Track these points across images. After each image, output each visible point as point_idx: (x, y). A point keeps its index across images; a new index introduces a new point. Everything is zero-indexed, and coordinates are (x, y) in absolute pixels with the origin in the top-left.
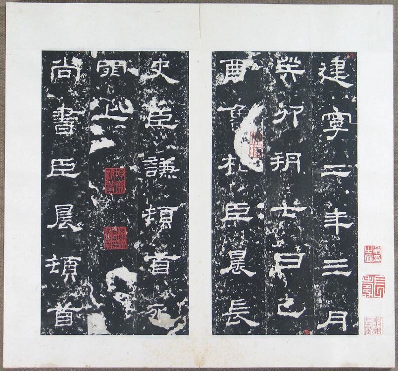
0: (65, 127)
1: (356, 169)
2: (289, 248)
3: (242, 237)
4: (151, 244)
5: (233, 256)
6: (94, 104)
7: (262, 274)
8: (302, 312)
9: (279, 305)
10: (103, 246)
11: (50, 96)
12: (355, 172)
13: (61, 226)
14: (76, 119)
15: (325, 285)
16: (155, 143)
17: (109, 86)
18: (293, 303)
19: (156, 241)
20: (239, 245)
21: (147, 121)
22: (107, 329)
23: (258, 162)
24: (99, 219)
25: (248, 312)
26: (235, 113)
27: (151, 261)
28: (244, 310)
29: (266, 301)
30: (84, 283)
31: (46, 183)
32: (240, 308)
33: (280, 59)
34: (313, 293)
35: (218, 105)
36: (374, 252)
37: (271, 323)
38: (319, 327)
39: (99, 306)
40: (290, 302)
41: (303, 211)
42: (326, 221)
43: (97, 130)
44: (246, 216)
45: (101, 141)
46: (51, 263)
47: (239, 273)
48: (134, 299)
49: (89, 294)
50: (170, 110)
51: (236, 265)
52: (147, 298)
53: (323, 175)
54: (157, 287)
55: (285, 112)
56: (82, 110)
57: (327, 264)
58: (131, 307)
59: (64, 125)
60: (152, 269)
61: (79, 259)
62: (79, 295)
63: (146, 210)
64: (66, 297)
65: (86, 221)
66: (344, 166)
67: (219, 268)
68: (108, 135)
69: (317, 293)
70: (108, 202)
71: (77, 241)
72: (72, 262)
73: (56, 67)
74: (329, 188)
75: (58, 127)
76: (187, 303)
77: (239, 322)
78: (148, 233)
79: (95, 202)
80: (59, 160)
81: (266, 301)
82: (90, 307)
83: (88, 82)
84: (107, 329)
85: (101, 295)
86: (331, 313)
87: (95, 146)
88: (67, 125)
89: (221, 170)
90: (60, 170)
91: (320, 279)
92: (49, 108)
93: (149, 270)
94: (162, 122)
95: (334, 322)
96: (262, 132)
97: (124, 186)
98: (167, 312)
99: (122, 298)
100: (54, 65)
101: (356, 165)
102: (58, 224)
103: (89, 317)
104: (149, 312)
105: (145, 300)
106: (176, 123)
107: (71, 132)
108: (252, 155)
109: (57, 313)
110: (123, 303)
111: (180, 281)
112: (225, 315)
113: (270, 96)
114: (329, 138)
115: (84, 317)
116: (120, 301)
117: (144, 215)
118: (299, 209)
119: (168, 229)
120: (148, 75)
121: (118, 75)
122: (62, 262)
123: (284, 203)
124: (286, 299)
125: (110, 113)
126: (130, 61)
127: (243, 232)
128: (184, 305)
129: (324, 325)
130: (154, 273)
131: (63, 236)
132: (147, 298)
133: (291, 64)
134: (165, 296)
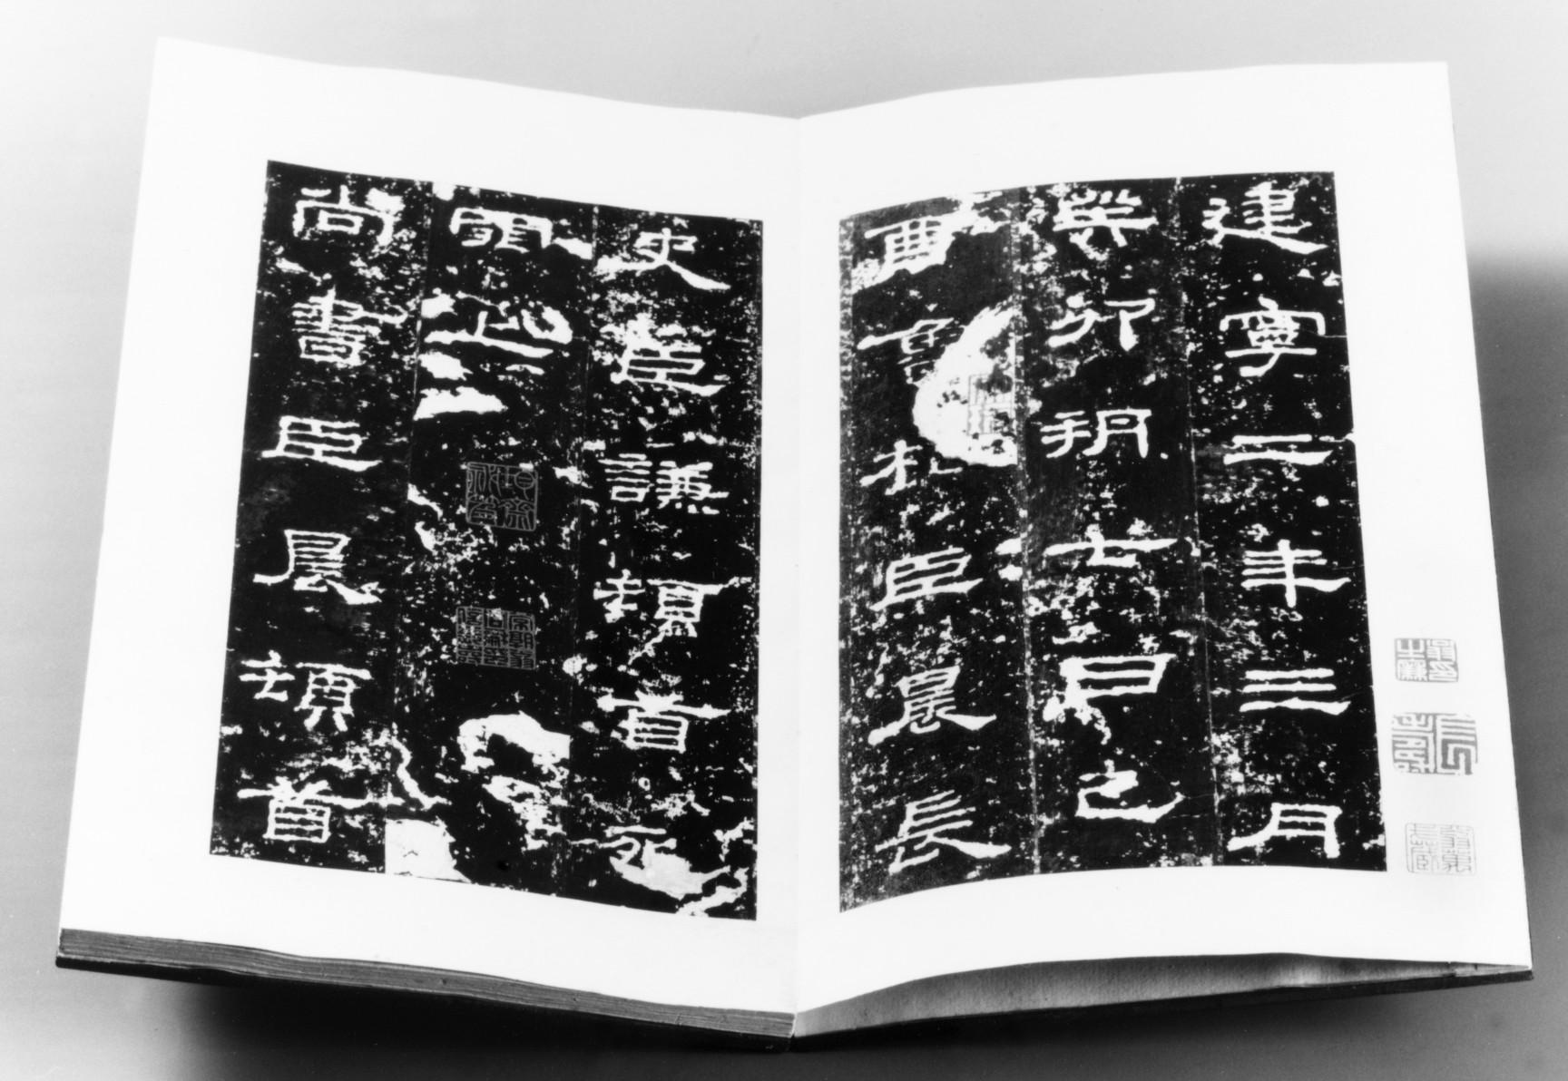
0: (335, 345)
1: (1350, 447)
2: (1116, 638)
3: (945, 635)
4: (622, 668)
5: (912, 690)
6: (438, 304)
7: (1012, 721)
8: (1166, 809)
9: (1082, 793)
10: (450, 651)
11: (286, 265)
12: (1346, 456)
13: (302, 584)
14: (375, 331)
15: (1255, 736)
16: (643, 421)
17: (491, 269)
18: (1136, 784)
19: (640, 663)
20: (933, 655)
21: (616, 367)
22: (456, 867)
23: (998, 444)
24: (440, 584)
25: (968, 823)
26: (916, 342)
27: (622, 713)
28: (955, 819)
29: (1033, 785)
30: (376, 736)
31: (255, 474)
32: (937, 817)
33: (1068, 197)
34: (1209, 756)
35: (859, 334)
36: (1428, 658)
37: (1052, 842)
38: (1236, 844)
39: (428, 802)
40: (1121, 781)
41: (1164, 551)
42: (1246, 572)
43: (444, 366)
44: (959, 579)
45: (455, 393)
46: (261, 672)
47: (936, 726)
48: (558, 801)
49: (394, 767)
50: (698, 349)
51: (924, 710)
52: (605, 807)
53: (1229, 459)
54: (643, 782)
55: (1091, 317)
56: (393, 312)
57: (1258, 682)
58: (545, 821)
59: (330, 340)
60: (625, 733)
61: (365, 675)
62: (359, 767)
63: (610, 581)
64: (309, 767)
65: (390, 579)
66: (1307, 438)
67: (865, 730)
68: (481, 382)
69: (1224, 755)
70: (475, 544)
71: (361, 630)
72: (340, 679)
73: (311, 204)
74: (1255, 492)
75: (309, 343)
76: (751, 834)
77: (936, 853)
78: (613, 642)
79: (428, 539)
80: (305, 421)
81: (1033, 785)
82: (399, 801)
83: (419, 252)
84: (456, 867)
85: (439, 776)
86: (1277, 808)
87: (433, 405)
88: (341, 341)
89: (872, 486)
90: (308, 445)
91: (1227, 715)
92: (281, 293)
93: (615, 734)
94: (669, 376)
95: (1290, 834)
96: (1010, 373)
97: (531, 515)
98: (679, 852)
99: (514, 794)
100: (307, 198)
101: (1349, 437)
102: (294, 576)
103: (391, 826)
104: (614, 845)
105: (599, 810)
106: (718, 383)
107: (354, 360)
108: (975, 429)
109: (273, 805)
110: (518, 807)
111: (728, 773)
112: (886, 845)
113: (1037, 284)
114: (1247, 371)
115: (372, 826)
116: (507, 801)
117: (599, 594)
118: (1148, 546)
119: (685, 637)
120: (625, 260)
121: (523, 250)
122: (302, 676)
123: (1093, 532)
124: (1108, 775)
125: (489, 333)
126: (564, 222)
127: (947, 621)
128: (739, 840)
129: (1257, 840)
130: (631, 744)
131: (309, 609)
132: (605, 807)
133: (1106, 206)
134: (673, 807)
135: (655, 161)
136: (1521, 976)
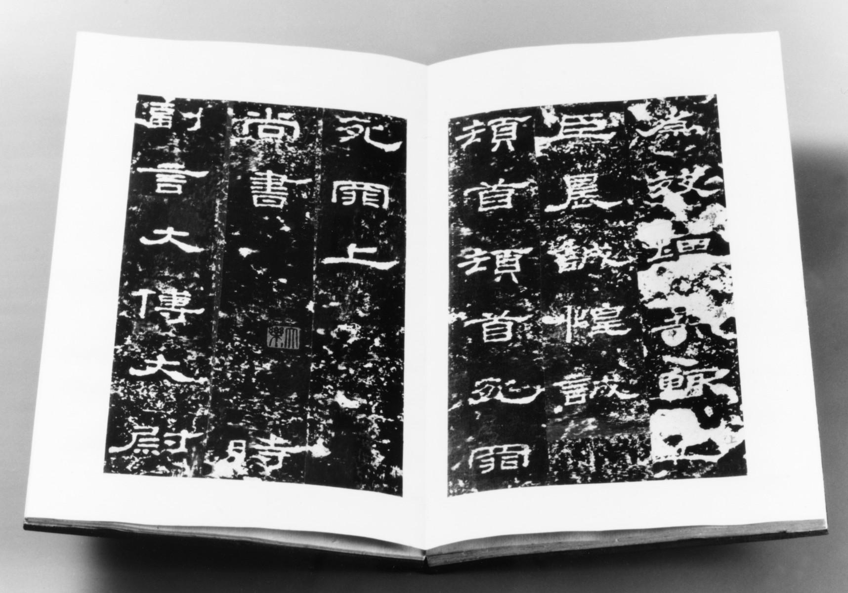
135: (349, 83)
136: (824, 532)
